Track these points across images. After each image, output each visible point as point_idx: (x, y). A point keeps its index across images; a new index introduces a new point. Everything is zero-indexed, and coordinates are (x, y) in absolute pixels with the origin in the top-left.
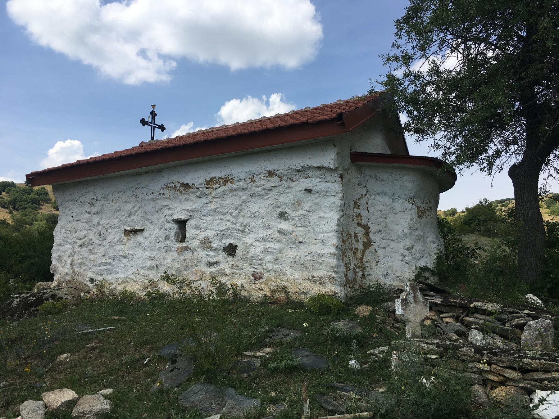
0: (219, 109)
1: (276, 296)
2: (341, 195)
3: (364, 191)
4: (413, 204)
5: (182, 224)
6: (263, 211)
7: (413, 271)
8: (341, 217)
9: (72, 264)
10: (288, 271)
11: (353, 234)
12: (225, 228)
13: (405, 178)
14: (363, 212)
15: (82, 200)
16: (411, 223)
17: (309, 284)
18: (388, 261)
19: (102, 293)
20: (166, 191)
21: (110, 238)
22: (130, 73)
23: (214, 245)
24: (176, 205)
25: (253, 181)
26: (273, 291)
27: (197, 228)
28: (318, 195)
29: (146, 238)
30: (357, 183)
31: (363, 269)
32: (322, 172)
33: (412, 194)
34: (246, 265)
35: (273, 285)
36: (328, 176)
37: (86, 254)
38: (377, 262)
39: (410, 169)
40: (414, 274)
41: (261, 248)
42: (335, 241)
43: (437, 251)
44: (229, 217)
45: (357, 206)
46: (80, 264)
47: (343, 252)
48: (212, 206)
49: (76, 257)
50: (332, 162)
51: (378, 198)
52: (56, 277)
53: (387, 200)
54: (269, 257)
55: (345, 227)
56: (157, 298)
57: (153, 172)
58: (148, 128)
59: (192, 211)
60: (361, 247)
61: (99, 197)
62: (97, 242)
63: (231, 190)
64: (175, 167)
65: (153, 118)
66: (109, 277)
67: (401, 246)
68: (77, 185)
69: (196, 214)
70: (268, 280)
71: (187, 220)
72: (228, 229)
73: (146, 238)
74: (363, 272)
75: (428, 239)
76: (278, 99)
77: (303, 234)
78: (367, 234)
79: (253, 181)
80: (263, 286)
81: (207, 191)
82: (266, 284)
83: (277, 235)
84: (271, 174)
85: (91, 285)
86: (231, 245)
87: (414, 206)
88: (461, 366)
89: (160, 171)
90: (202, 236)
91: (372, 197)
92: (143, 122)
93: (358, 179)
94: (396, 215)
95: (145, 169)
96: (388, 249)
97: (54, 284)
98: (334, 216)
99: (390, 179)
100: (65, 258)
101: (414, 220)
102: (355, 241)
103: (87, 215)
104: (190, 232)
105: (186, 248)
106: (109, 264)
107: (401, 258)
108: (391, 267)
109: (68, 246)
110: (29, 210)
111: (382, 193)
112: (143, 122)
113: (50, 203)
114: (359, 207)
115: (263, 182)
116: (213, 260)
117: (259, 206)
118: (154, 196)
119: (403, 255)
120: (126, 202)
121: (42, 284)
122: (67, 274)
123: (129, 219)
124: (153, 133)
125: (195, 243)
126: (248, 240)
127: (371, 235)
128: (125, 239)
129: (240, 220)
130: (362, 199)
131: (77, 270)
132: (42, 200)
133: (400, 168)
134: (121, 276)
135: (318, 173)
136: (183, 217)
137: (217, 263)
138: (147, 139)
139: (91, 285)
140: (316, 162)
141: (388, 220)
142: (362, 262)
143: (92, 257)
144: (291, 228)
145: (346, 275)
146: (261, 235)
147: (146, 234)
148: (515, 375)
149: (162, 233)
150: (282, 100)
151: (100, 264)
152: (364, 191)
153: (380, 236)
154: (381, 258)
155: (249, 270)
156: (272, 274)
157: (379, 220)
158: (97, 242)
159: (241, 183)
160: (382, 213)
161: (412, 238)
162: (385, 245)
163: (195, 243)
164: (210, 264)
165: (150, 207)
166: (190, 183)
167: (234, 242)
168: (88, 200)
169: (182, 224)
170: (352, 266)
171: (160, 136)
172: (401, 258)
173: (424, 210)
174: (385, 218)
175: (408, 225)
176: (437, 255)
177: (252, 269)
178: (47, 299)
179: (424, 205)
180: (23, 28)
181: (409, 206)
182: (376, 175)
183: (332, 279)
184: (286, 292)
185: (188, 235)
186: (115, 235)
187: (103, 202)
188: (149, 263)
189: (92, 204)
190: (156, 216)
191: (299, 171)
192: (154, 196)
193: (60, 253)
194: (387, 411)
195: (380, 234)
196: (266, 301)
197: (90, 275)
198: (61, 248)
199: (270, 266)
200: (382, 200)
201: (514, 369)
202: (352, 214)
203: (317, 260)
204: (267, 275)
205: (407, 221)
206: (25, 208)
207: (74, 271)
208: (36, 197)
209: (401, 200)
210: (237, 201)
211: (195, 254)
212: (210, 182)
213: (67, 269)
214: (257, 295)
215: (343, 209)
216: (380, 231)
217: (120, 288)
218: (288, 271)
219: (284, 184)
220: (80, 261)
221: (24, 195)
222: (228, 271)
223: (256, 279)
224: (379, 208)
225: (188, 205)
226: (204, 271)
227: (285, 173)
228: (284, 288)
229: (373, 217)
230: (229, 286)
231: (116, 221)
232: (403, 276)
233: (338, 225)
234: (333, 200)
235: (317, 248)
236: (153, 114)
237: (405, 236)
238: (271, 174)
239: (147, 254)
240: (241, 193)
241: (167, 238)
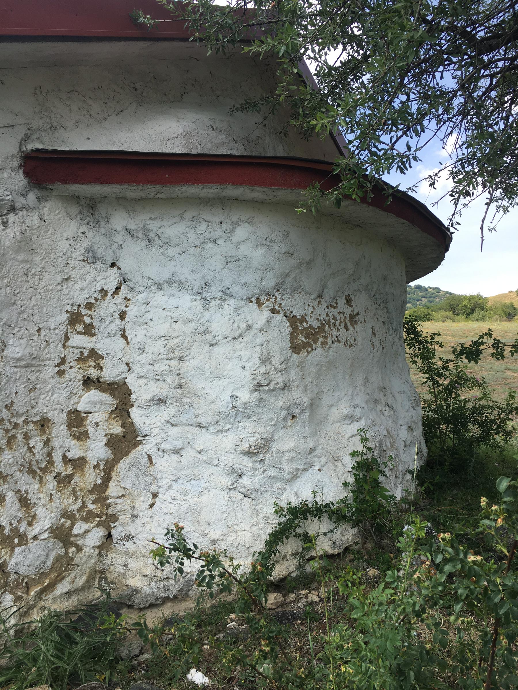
4: (273, 311)
7: (266, 519)
11: (60, 419)
13: (242, 232)
14: (106, 344)
16: (263, 370)
18: (187, 493)
31: (108, 521)
33: (269, 282)
38: (155, 495)
39: (257, 205)
40: (269, 530)
43: (360, 448)
45: (80, 328)
51: (159, 299)
53: (186, 302)
60: (97, 450)
67: (227, 444)
74: (109, 529)
75: (334, 410)
78: (122, 409)
87: (279, 318)
91: (141, 297)
93: (86, 244)
94: (215, 349)
96: (189, 455)
99: (192, 236)
101: (276, 361)
107: (227, 481)
111: (170, 282)
119: (233, 471)
127: (135, 413)
130: (103, 304)
133: (223, 203)
141: (189, 365)
153: (165, 413)
154: (165, 482)
157: (160, 367)
160: (171, 343)
161: (265, 417)
162: (179, 444)
172: (227, 481)
173: (321, 329)
174: (181, 359)
175: (249, 377)
176: (359, 459)
179: (321, 311)
181: (260, 317)
182: (146, 230)
194: (480, 445)
195: (162, 408)
200: (173, 302)
205: (248, 365)
209: (232, 302)
229: (144, 359)
232: (231, 539)
237: (240, 412)
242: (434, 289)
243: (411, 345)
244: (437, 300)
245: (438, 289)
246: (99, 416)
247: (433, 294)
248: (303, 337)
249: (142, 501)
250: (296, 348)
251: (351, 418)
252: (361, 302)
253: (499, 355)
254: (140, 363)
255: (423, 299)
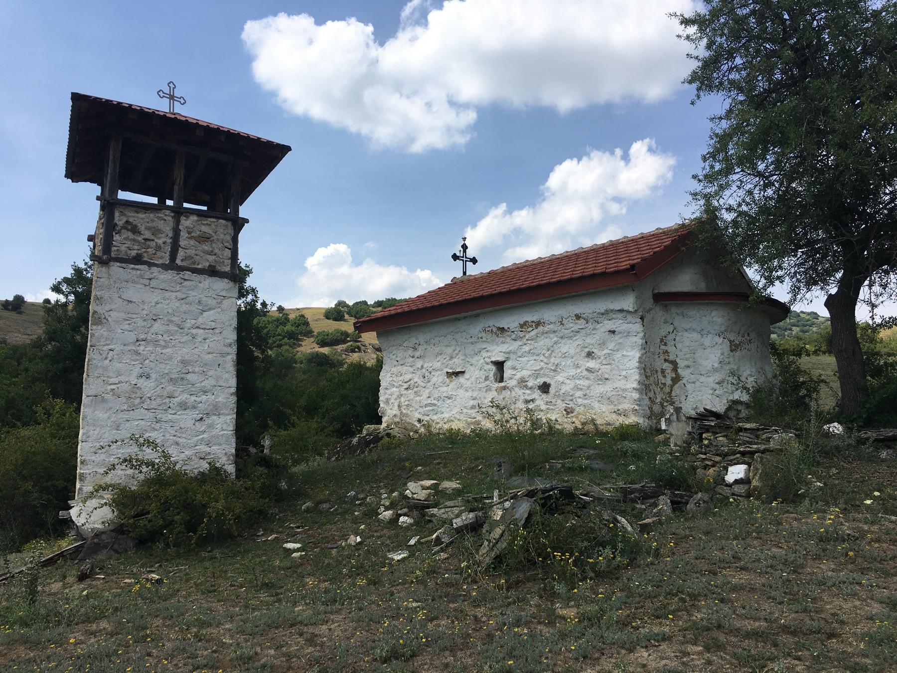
0: (546, 177)
1: (586, 428)
2: (642, 335)
3: (671, 328)
5: (500, 365)
6: (572, 351)
8: (642, 355)
9: (399, 406)
10: (596, 405)
11: (659, 370)
12: (538, 368)
13: (714, 313)
14: (670, 348)
15: (405, 344)
17: (614, 416)
19: (430, 432)
20: (483, 334)
21: (434, 380)
22: (413, 140)
23: (530, 384)
24: (493, 348)
25: (562, 324)
26: (583, 424)
27: (514, 368)
28: (620, 335)
29: (468, 379)
30: (662, 321)
32: (624, 314)
33: (723, 329)
34: (559, 401)
35: (583, 418)
36: (630, 318)
37: (412, 396)
41: (572, 386)
42: (637, 377)
44: (542, 358)
46: (408, 405)
47: (645, 387)
48: (527, 348)
49: (403, 399)
50: (631, 305)
51: (686, 334)
52: (384, 420)
53: (695, 335)
54: (579, 394)
55: (648, 365)
56: (480, 435)
57: (471, 316)
58: (459, 263)
59: (508, 353)
60: (669, 382)
61: (422, 342)
62: (423, 384)
63: (543, 333)
64: (491, 312)
65: (465, 251)
66: (435, 417)
67: (711, 380)
68: (399, 330)
69: (511, 356)
70: (579, 414)
71: (504, 362)
72: (542, 369)
73: (468, 379)
76: (645, 149)
77: (608, 371)
78: (675, 369)
79: (562, 324)
80: (574, 419)
81: (522, 334)
82: (577, 417)
83: (585, 373)
84: (578, 317)
85: (418, 425)
86: (545, 383)
88: (693, 458)
89: (477, 316)
90: (519, 375)
92: (455, 257)
95: (463, 314)
96: (698, 384)
97: (384, 425)
98: (636, 354)
100: (392, 401)
102: (659, 378)
103: (412, 359)
104: (507, 373)
105: (504, 388)
106: (435, 405)
107: (711, 392)
108: (701, 401)
109: (394, 389)
110: (285, 348)
112: (455, 257)
113: (312, 336)
114: (665, 344)
115: (571, 325)
116: (529, 398)
117: (570, 347)
118: (473, 340)
120: (447, 346)
121: (368, 428)
122: (395, 416)
123: (450, 362)
124: (465, 267)
125: (512, 383)
126: (560, 378)
127: (679, 370)
128: (448, 380)
129: (552, 360)
131: (404, 411)
132: (301, 333)
133: (708, 304)
134: (446, 416)
135: (620, 315)
136: (501, 359)
137: (533, 400)
138: (459, 275)
139: (418, 425)
140: (617, 306)
141: (697, 355)
142: (670, 396)
143: (418, 398)
144: (597, 366)
145: (650, 408)
146: (571, 374)
147: (467, 375)
148: (718, 459)
149: (482, 374)
150: (650, 150)
151: (426, 406)
152: (671, 328)
155: (561, 405)
156: (582, 408)
157: (688, 356)
158: (423, 384)
159: (551, 326)
163: (512, 383)
164: (527, 402)
165: (469, 350)
166: (506, 327)
167: (548, 381)
168: (411, 345)
169: (500, 365)
170: (658, 400)
171: (473, 270)
172: (711, 392)
177: (564, 405)
178: (382, 437)
179: (740, 338)
180: (273, 94)
181: (720, 340)
183: (634, 410)
184: (595, 424)
185: (505, 376)
186: (439, 377)
187: (425, 346)
188: (472, 403)
189: (415, 349)
190: (476, 358)
191: (603, 314)
192: (473, 340)
193: (387, 396)
196: (576, 432)
197: (417, 416)
198: (388, 392)
199: (580, 401)
200: (691, 336)
201: (717, 455)
202: (658, 350)
203: (621, 394)
204: (577, 409)
206: (280, 346)
207: (401, 413)
208: (293, 328)
210: (548, 342)
211: (513, 393)
212: (523, 326)
213: (395, 411)
214: (569, 428)
215: (646, 345)
216: (688, 367)
217: (446, 426)
218: (596, 405)
219: (590, 325)
220: (407, 403)
221: (277, 327)
222: (543, 407)
223: (568, 413)
224: (688, 344)
225: (505, 348)
226: (520, 404)
227: (590, 316)
228: (593, 420)
230: (545, 421)
231: (439, 364)
233: (640, 362)
234: (635, 339)
235: (621, 384)
236: (465, 247)
237: (715, 370)
238: (578, 317)
239: (469, 394)
240: (552, 336)
241: (487, 378)
242: (809, 314)
243: (773, 355)
244: (815, 329)
245: (816, 314)
246: (668, 371)
247: (808, 320)
248: (734, 347)
249: (683, 398)
250: (732, 351)
251: (751, 376)
252: (753, 335)
253: (808, 355)
254: (681, 355)
255: (794, 328)
